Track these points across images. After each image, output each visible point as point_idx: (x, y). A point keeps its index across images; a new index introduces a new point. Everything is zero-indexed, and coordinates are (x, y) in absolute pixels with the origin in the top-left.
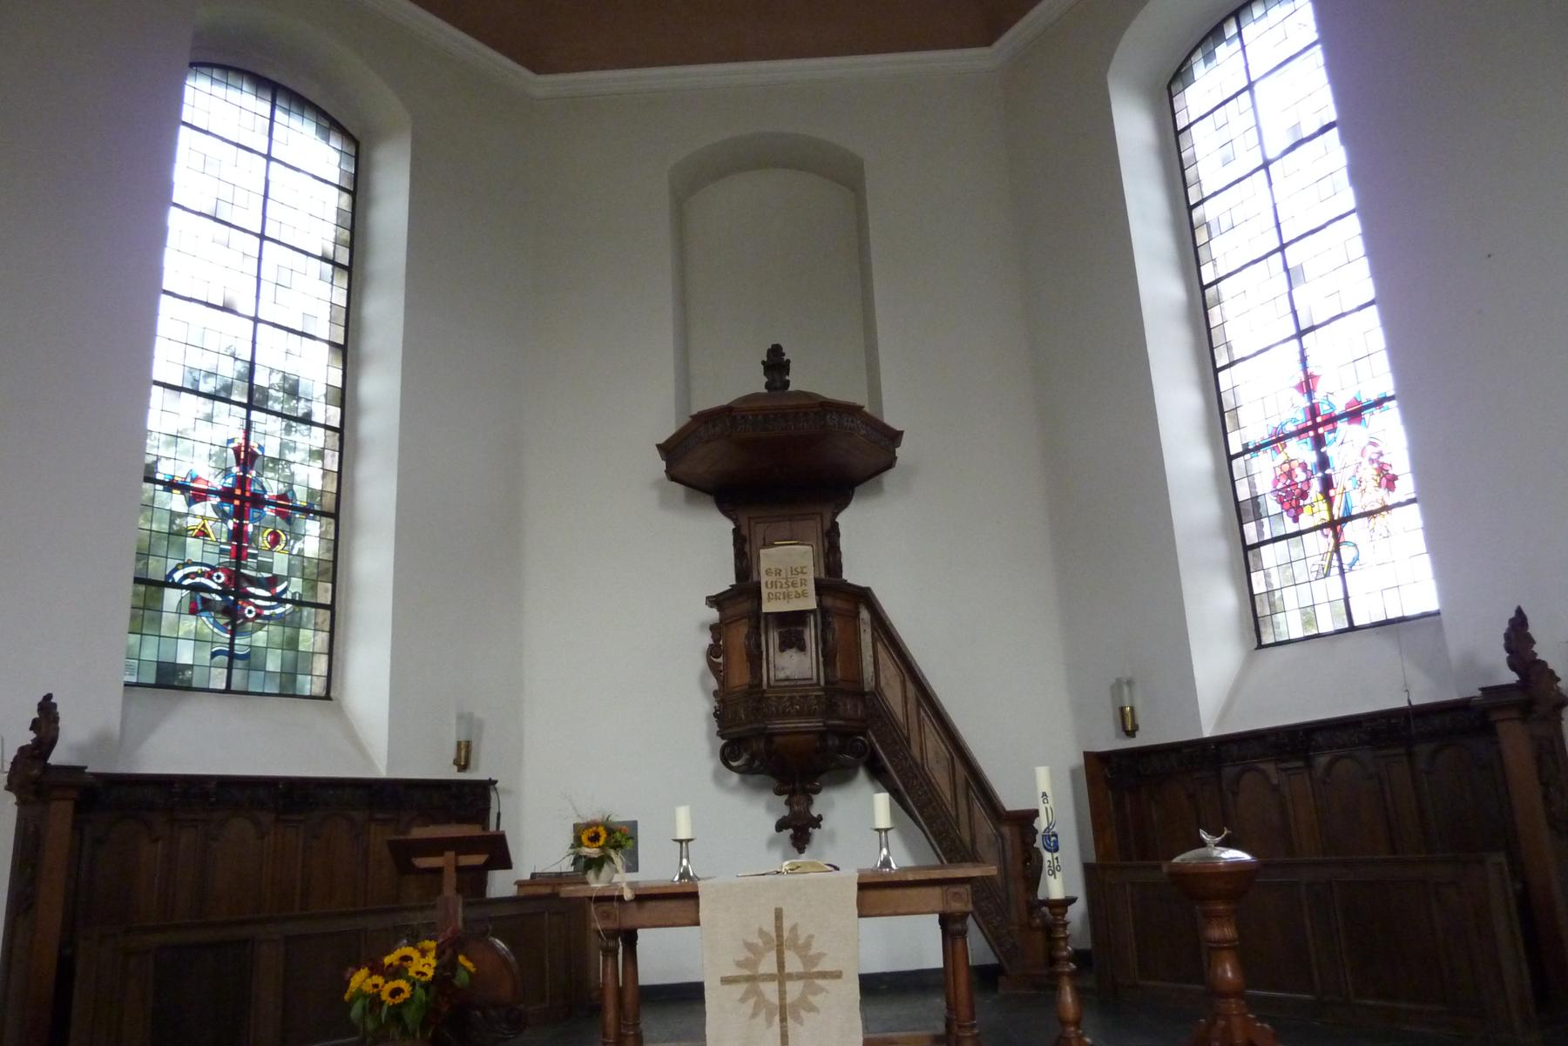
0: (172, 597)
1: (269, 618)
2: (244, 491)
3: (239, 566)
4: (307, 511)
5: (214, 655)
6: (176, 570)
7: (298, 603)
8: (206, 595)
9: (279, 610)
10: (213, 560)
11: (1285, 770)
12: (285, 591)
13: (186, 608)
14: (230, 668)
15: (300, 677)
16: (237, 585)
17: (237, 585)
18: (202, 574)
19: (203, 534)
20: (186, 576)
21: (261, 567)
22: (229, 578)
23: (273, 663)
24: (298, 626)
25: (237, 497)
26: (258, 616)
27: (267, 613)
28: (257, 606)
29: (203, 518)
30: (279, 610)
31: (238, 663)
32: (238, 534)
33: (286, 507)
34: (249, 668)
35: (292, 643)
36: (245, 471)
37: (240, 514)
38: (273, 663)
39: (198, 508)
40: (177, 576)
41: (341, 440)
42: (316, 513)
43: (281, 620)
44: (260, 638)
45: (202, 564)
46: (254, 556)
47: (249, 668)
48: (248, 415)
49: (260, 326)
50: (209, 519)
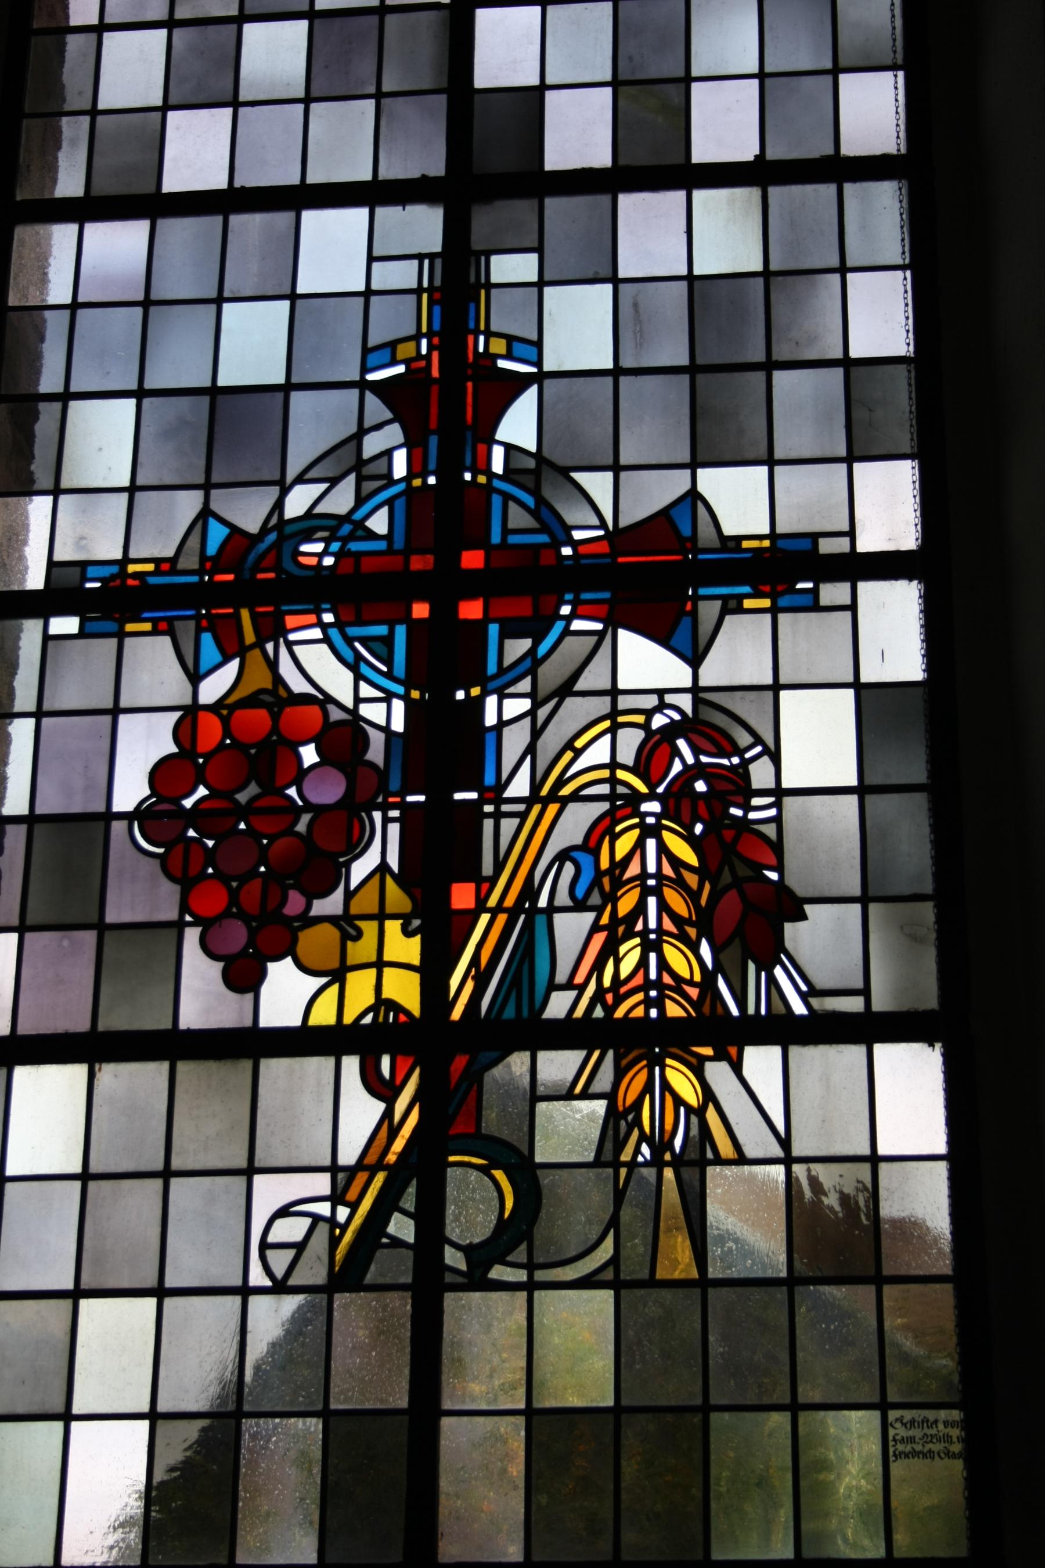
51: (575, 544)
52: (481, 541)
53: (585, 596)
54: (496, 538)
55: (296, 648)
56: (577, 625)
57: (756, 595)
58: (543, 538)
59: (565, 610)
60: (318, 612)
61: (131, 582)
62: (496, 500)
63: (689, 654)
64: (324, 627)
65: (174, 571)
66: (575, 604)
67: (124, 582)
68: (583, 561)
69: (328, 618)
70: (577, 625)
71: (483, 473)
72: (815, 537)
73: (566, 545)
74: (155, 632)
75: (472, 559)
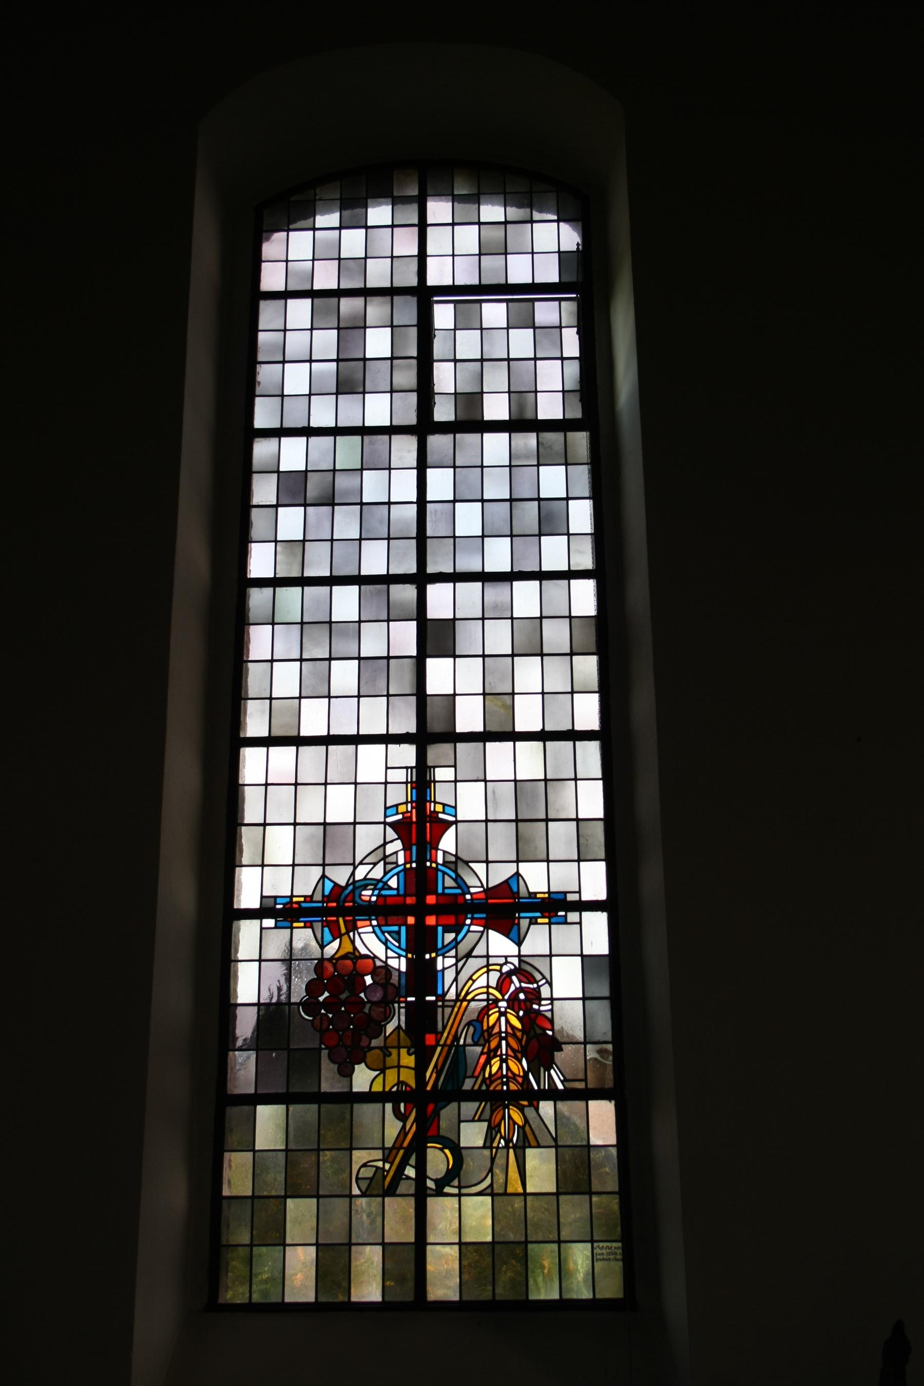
51: (471, 894)
52: (434, 891)
56: (473, 928)
58: (459, 891)
60: (472, 899)
65: (311, 901)
66: (472, 919)
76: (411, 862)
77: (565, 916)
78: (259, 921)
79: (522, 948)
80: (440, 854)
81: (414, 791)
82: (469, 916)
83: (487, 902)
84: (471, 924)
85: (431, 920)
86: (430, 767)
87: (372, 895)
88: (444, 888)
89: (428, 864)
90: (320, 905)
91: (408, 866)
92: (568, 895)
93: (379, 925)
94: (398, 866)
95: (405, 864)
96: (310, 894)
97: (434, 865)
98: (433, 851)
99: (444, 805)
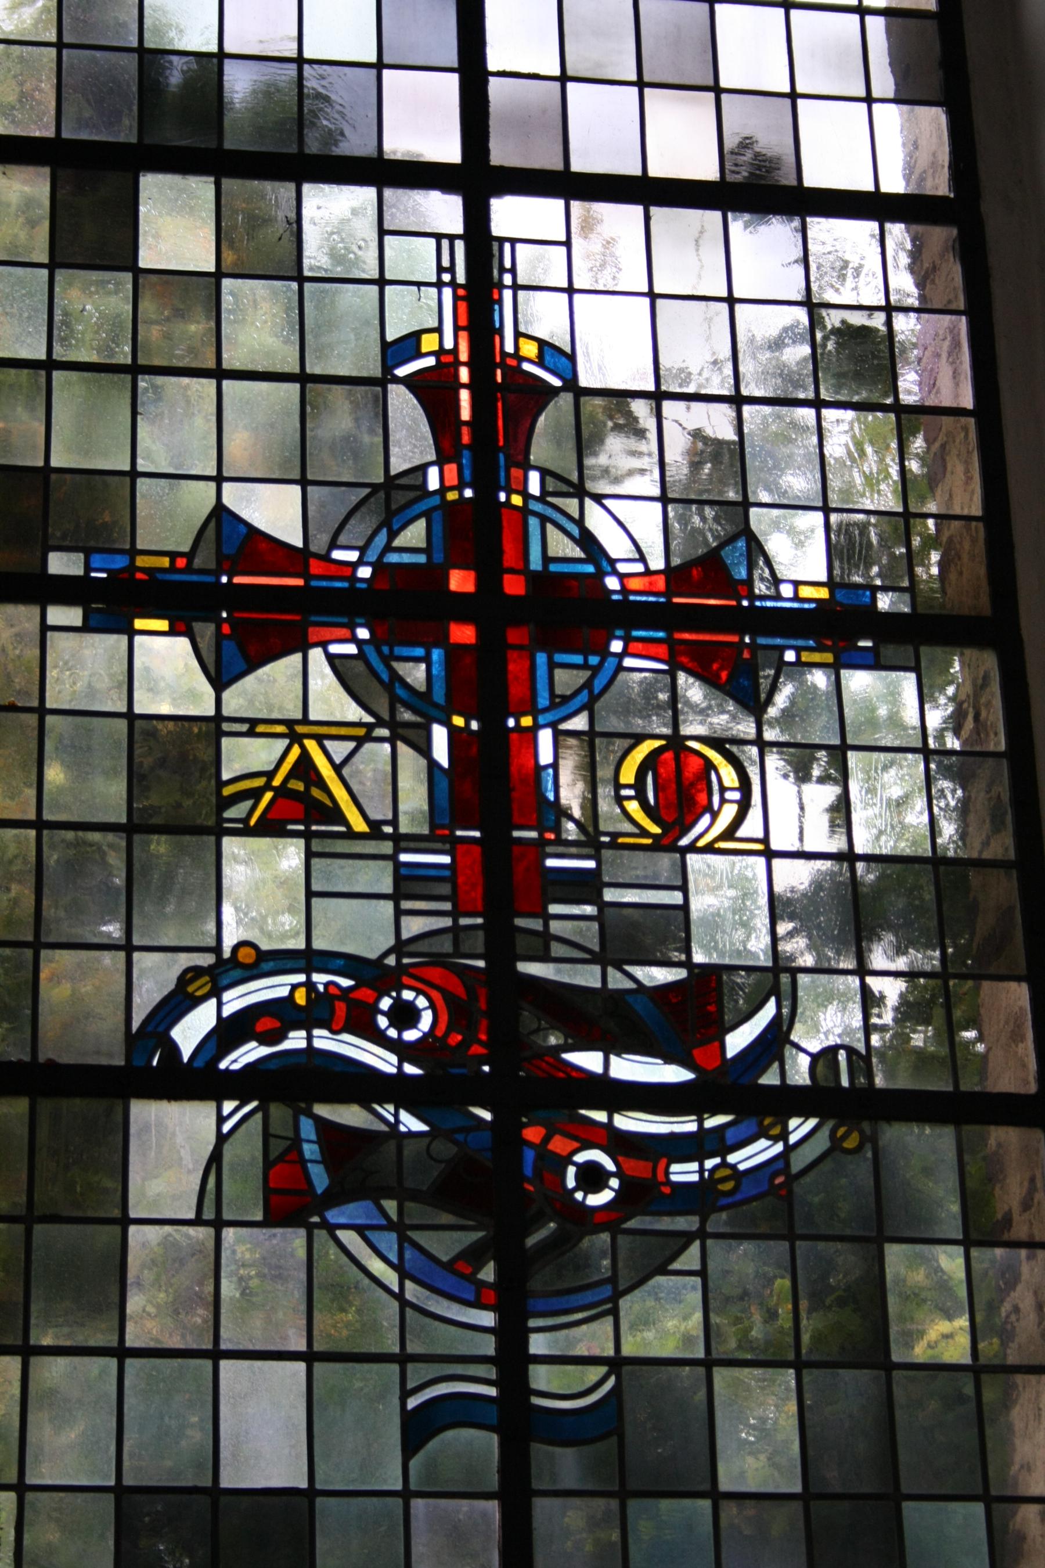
0: (172, 1145)
1: (697, 1198)
2: (489, 574)
3: (503, 945)
4: (840, 627)
5: (418, 1428)
6: (178, 1002)
7: (845, 1097)
8: (350, 1115)
9: (752, 1155)
10: (363, 928)
11: (1024, 1387)
12: (775, 1042)
13: (244, 1194)
14: (516, 1493)
15: (916, 1515)
16: (503, 1048)
17: (510, 1045)
18: (318, 1011)
19: (298, 808)
20: (229, 1032)
21: (627, 937)
22: (455, 1011)
23: (759, 1436)
24: (884, 1221)
25: (462, 607)
26: (639, 1194)
27: (684, 1172)
28: (620, 1144)
29: (294, 730)
30: (752, 1155)
31: (562, 1464)
32: (489, 789)
33: (715, 615)
34: (625, 1486)
35: (862, 1335)
36: (487, 481)
37: (485, 690)
38: (759, 1436)
39: (271, 686)
40: (191, 1031)
41: (973, 254)
42: (888, 628)
43: (771, 1205)
44: (665, 1321)
45: (308, 959)
46: (584, 887)
47: (625, 1486)
48: (477, 219)
49: (738, 307)
50: (328, 731)
51: (354, 639)
52: (454, 654)
53: (636, 633)
54: (437, 654)
55: (637, 556)
56: (353, 556)
57: (820, 649)
58: (590, 569)
59: (364, 572)
60: (352, 627)
61: (139, 576)
62: (533, 523)
63: (224, 514)
64: (360, 643)
65: (189, 569)
66: (627, 640)
67: (133, 575)
68: (345, 620)
69: (363, 633)
70: (353, 556)
71: (518, 492)
72: (87, 628)
73: (364, 641)
74: (172, 632)
75: (464, 634)
76: (460, 488)
77: (88, 568)
78: (36, 610)
79: (213, 501)
80: (534, 477)
81: (463, 306)
82: (619, 633)
83: (669, 602)
84: (625, 653)
85: (460, 581)
86: (502, 240)
87: (360, 562)
88: (547, 559)
89: (503, 497)
90: (762, 641)
91: (527, 721)
92: (79, 623)
93: (600, 574)
94: (553, 725)
95: (536, 727)
96: (186, 548)
97: (517, 500)
98: (516, 472)
99: (542, 344)
